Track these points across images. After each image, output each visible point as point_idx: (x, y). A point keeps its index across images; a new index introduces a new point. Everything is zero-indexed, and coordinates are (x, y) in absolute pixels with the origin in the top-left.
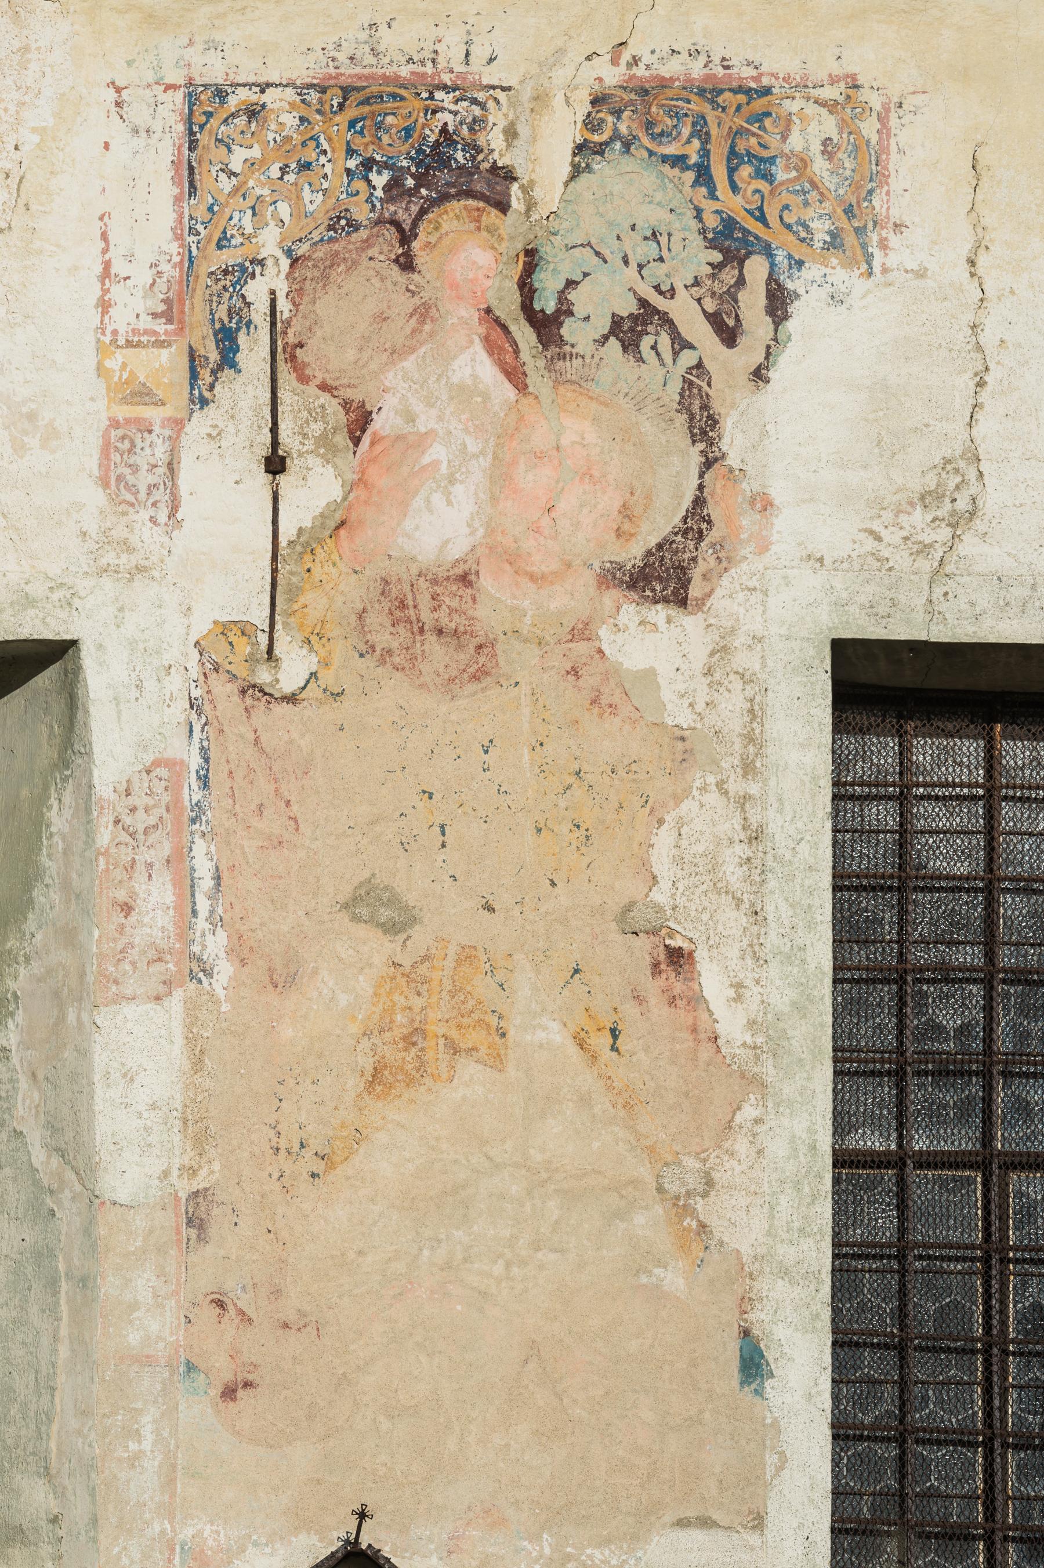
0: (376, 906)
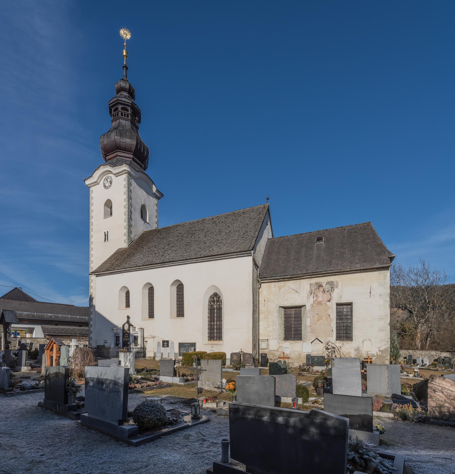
0: (318, 314)
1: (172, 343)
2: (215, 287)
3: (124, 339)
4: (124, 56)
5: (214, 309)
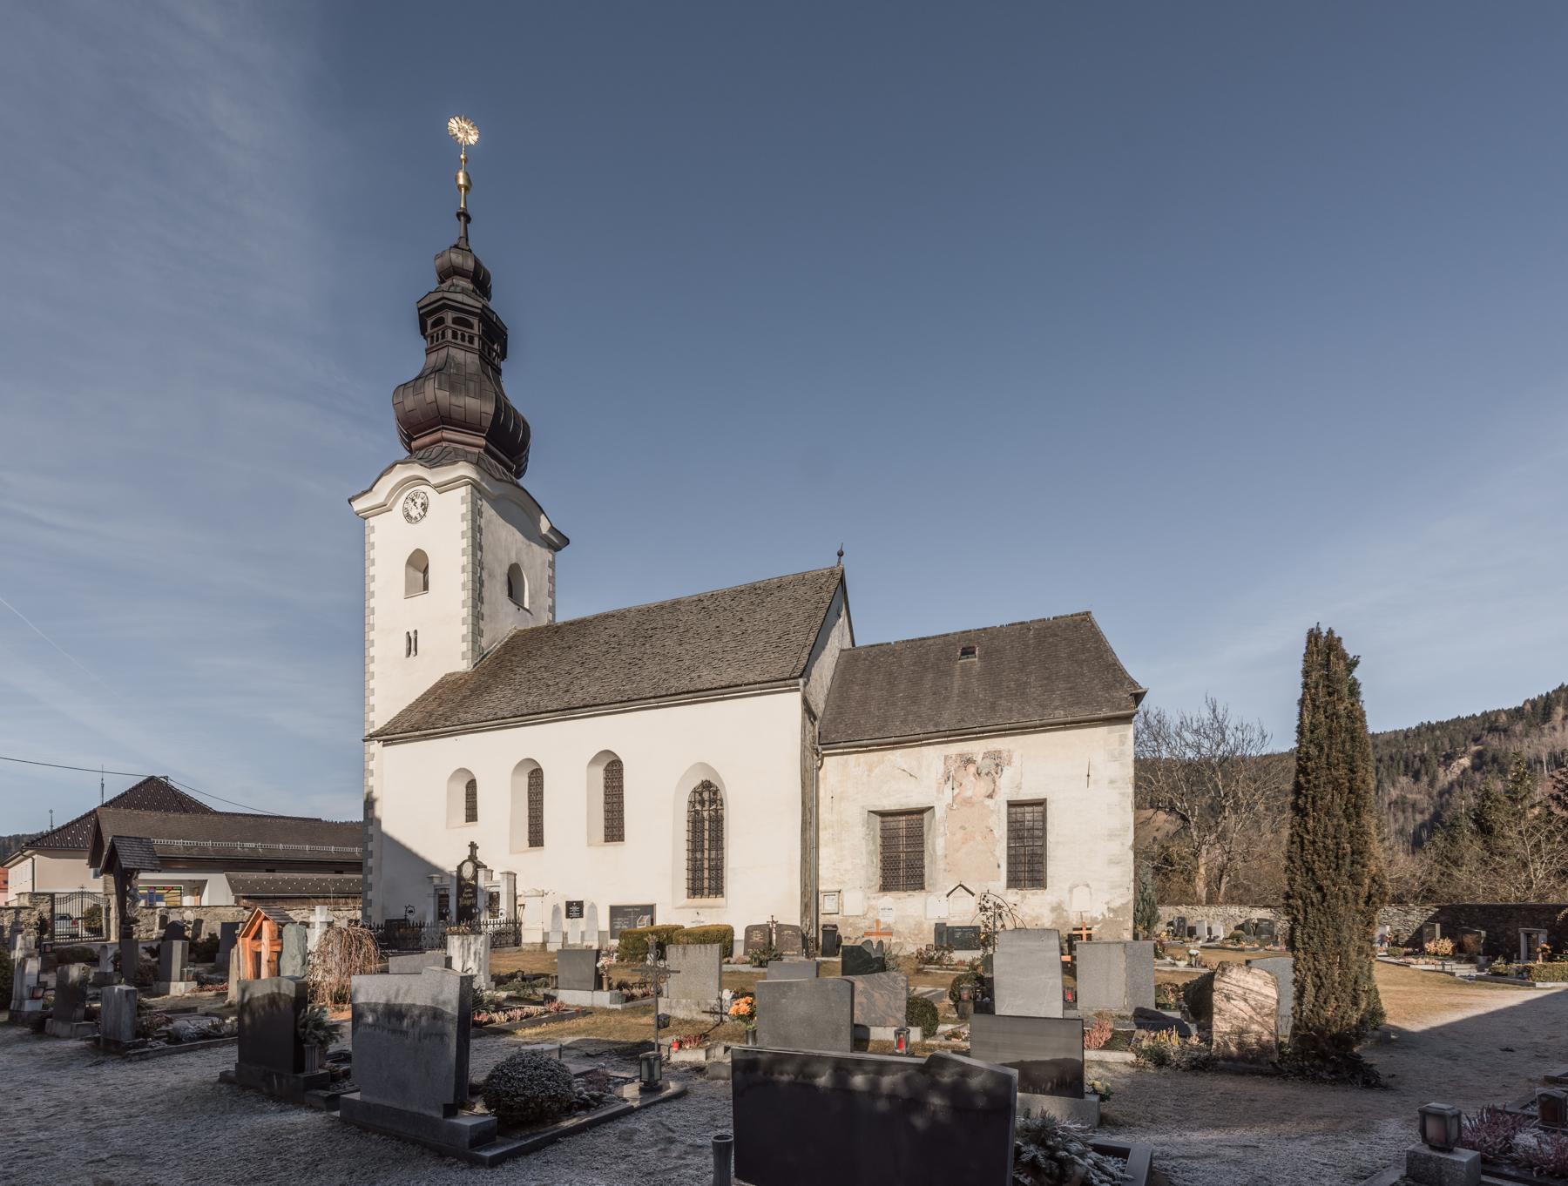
0: (963, 828)
1: (593, 906)
2: (705, 766)
3: (463, 901)
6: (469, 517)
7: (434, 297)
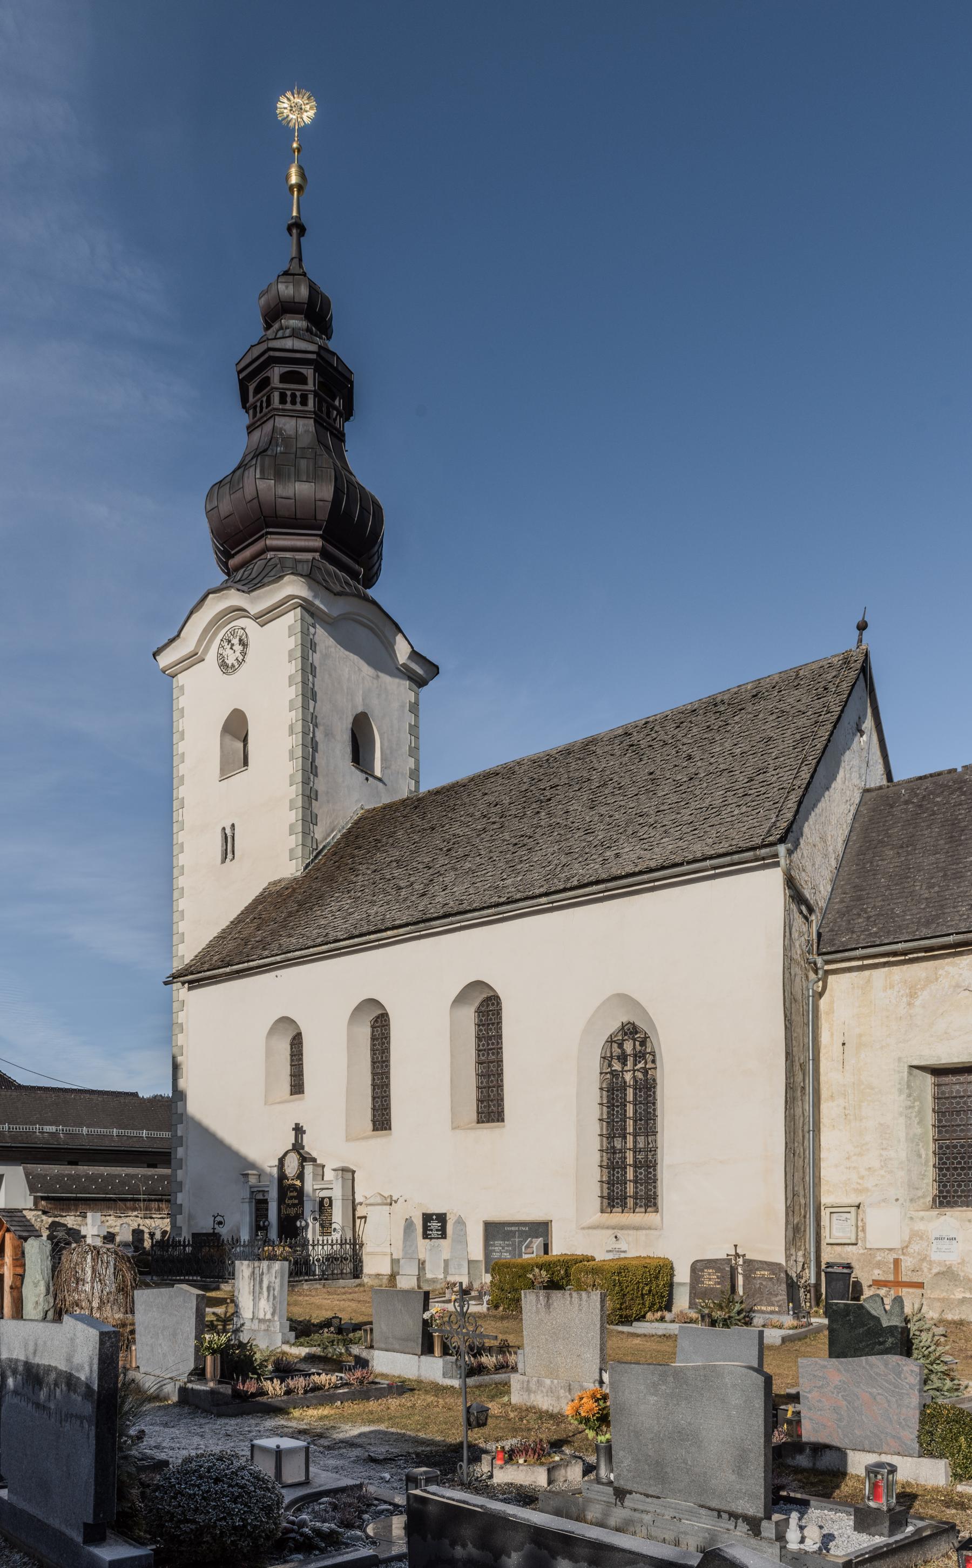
1: (460, 1222)
2: (625, 1000)
3: (284, 1212)
4: (291, 188)
5: (624, 1087)
6: (298, 654)
7: (256, 352)
